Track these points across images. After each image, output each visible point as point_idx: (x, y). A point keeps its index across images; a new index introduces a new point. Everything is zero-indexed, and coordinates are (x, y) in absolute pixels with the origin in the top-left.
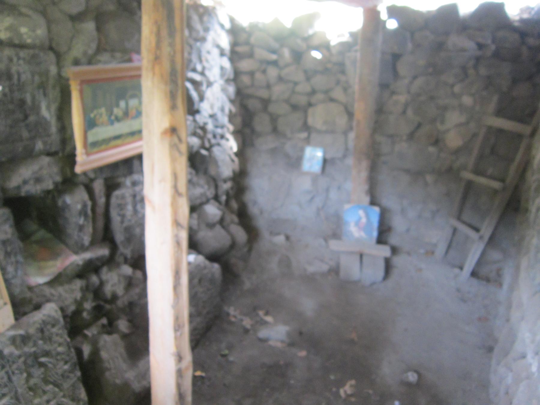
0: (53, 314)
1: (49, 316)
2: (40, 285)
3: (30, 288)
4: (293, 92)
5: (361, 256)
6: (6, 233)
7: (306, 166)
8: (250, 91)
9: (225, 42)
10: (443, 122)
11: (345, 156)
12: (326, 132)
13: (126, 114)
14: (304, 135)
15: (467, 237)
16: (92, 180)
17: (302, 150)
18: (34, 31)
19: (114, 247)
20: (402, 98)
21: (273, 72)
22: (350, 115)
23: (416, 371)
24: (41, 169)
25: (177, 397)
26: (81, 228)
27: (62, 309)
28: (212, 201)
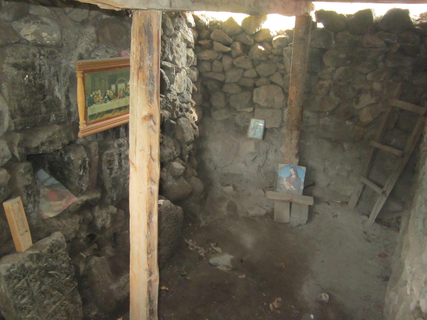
0: (60, 239)
1: (57, 241)
2: (51, 218)
3: (44, 221)
4: (243, 77)
5: (291, 203)
6: (29, 180)
7: (251, 134)
8: (209, 75)
9: (191, 36)
10: (357, 102)
11: (281, 127)
12: (267, 108)
13: (116, 95)
14: (250, 109)
15: (374, 192)
16: (89, 142)
17: (249, 121)
18: (51, 35)
19: (104, 191)
20: (326, 83)
21: (227, 61)
22: (286, 94)
23: (329, 295)
24: (53, 134)
25: (148, 301)
26: (81, 177)
27: (65, 236)
28: (178, 159)
